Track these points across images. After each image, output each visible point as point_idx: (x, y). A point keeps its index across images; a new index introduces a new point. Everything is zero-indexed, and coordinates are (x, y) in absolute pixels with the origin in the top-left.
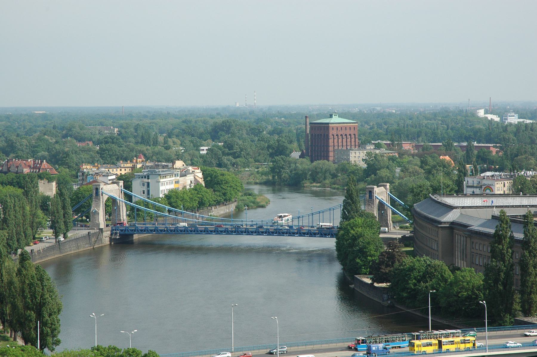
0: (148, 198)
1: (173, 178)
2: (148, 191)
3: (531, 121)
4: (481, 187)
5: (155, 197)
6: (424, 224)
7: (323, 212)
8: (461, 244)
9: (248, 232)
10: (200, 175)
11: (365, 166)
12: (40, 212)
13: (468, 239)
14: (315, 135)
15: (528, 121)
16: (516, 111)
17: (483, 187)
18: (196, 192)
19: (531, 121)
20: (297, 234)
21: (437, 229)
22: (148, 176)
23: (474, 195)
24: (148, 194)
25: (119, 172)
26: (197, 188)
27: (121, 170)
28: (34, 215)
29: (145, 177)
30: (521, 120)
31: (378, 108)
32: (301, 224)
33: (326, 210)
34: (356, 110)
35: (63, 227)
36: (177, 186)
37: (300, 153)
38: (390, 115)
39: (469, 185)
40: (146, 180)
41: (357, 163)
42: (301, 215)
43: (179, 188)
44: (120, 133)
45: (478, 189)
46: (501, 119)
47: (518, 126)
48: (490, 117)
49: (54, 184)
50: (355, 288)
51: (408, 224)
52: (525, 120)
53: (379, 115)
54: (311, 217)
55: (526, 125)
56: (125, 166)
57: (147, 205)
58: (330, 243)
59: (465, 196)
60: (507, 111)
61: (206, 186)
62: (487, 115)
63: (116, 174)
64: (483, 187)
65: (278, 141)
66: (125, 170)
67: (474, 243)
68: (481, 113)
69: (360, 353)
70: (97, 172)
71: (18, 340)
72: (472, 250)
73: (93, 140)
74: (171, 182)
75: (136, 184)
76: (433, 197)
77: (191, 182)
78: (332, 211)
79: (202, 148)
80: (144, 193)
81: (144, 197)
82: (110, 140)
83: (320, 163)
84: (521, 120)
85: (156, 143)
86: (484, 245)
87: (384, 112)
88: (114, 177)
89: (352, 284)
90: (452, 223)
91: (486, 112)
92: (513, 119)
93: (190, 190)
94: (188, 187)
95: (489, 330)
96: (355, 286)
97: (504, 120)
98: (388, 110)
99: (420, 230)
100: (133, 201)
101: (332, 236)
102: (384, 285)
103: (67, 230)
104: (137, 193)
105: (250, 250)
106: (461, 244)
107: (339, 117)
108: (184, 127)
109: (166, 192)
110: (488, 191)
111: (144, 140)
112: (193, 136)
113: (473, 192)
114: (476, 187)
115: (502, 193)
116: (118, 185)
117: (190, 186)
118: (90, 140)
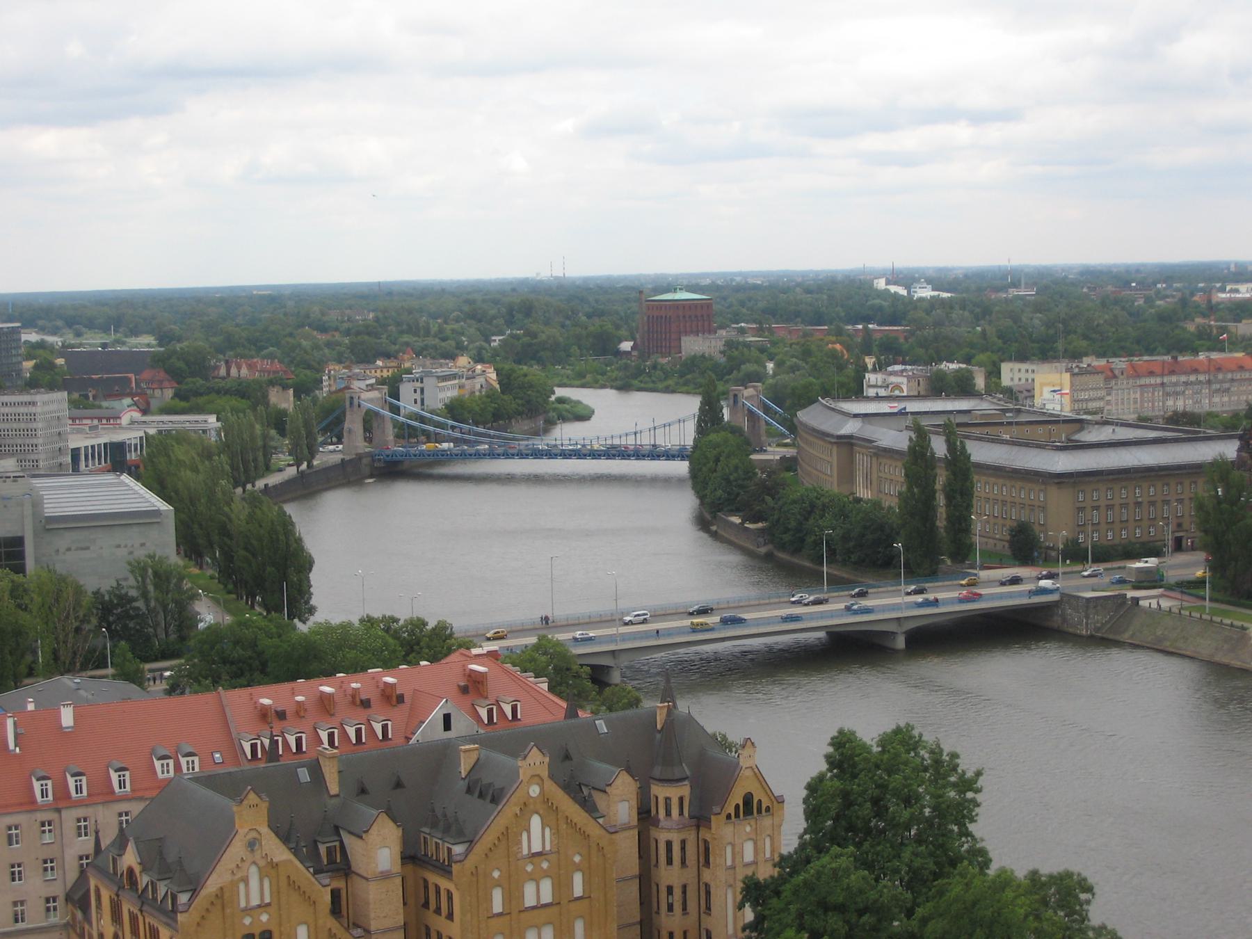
0: (423, 410)
1: (457, 381)
2: (422, 400)
3: (949, 295)
4: (888, 387)
5: (431, 408)
6: (811, 439)
7: (669, 425)
8: (863, 466)
9: (566, 455)
10: (493, 376)
11: (723, 360)
12: (273, 432)
13: (874, 459)
14: (657, 317)
15: (945, 295)
16: (929, 281)
17: (891, 387)
18: (489, 400)
19: (949, 295)
20: (634, 456)
21: (830, 446)
22: (422, 379)
23: (878, 398)
24: (422, 403)
25: (379, 374)
26: (491, 395)
27: (376, 372)
28: (265, 437)
29: (417, 381)
30: (936, 293)
31: (738, 279)
32: (639, 443)
33: (674, 423)
34: (708, 281)
35: (306, 451)
36: (462, 392)
37: (632, 343)
38: (756, 287)
39: (871, 383)
40: (418, 385)
41: (713, 354)
42: (638, 429)
43: (464, 395)
44: (377, 320)
45: (883, 390)
46: (909, 292)
47: (934, 303)
48: (893, 289)
49: (291, 391)
50: (719, 531)
51: (788, 441)
52: (941, 293)
53: (739, 288)
54: (652, 432)
55: (943, 300)
56: (388, 365)
57: (422, 419)
58: (681, 468)
59: (868, 399)
60: (917, 280)
61: (503, 392)
62: (889, 287)
63: (376, 377)
64: (891, 387)
65: (601, 326)
66: (388, 371)
67: (883, 465)
68: (881, 284)
69: (962, 600)
70: (350, 374)
71: (256, 607)
72: (880, 474)
73: (341, 329)
74: (453, 387)
75: (406, 390)
76: (824, 402)
77: (481, 386)
78: (682, 424)
79: (493, 338)
80: (416, 402)
81: (416, 409)
82: (368, 331)
83: (535, 341)
84: (936, 293)
85: (427, 333)
86: (896, 467)
87: (747, 283)
88: (373, 381)
89: (713, 525)
90: (851, 437)
91: (888, 283)
92: (925, 292)
93: (480, 398)
94: (477, 394)
95: (907, 583)
96: (718, 527)
97: (912, 294)
98: (750, 281)
99: (807, 448)
100: (401, 414)
101: (683, 458)
102: (760, 525)
103: (313, 457)
104: (408, 403)
105: (509, 479)
106: (863, 466)
107: (687, 291)
108: (466, 308)
109: (447, 401)
110: (897, 393)
111: (413, 329)
112: (480, 321)
113: (877, 394)
114: (881, 387)
115: (916, 394)
116: (381, 393)
117: (480, 392)
118: (337, 329)
